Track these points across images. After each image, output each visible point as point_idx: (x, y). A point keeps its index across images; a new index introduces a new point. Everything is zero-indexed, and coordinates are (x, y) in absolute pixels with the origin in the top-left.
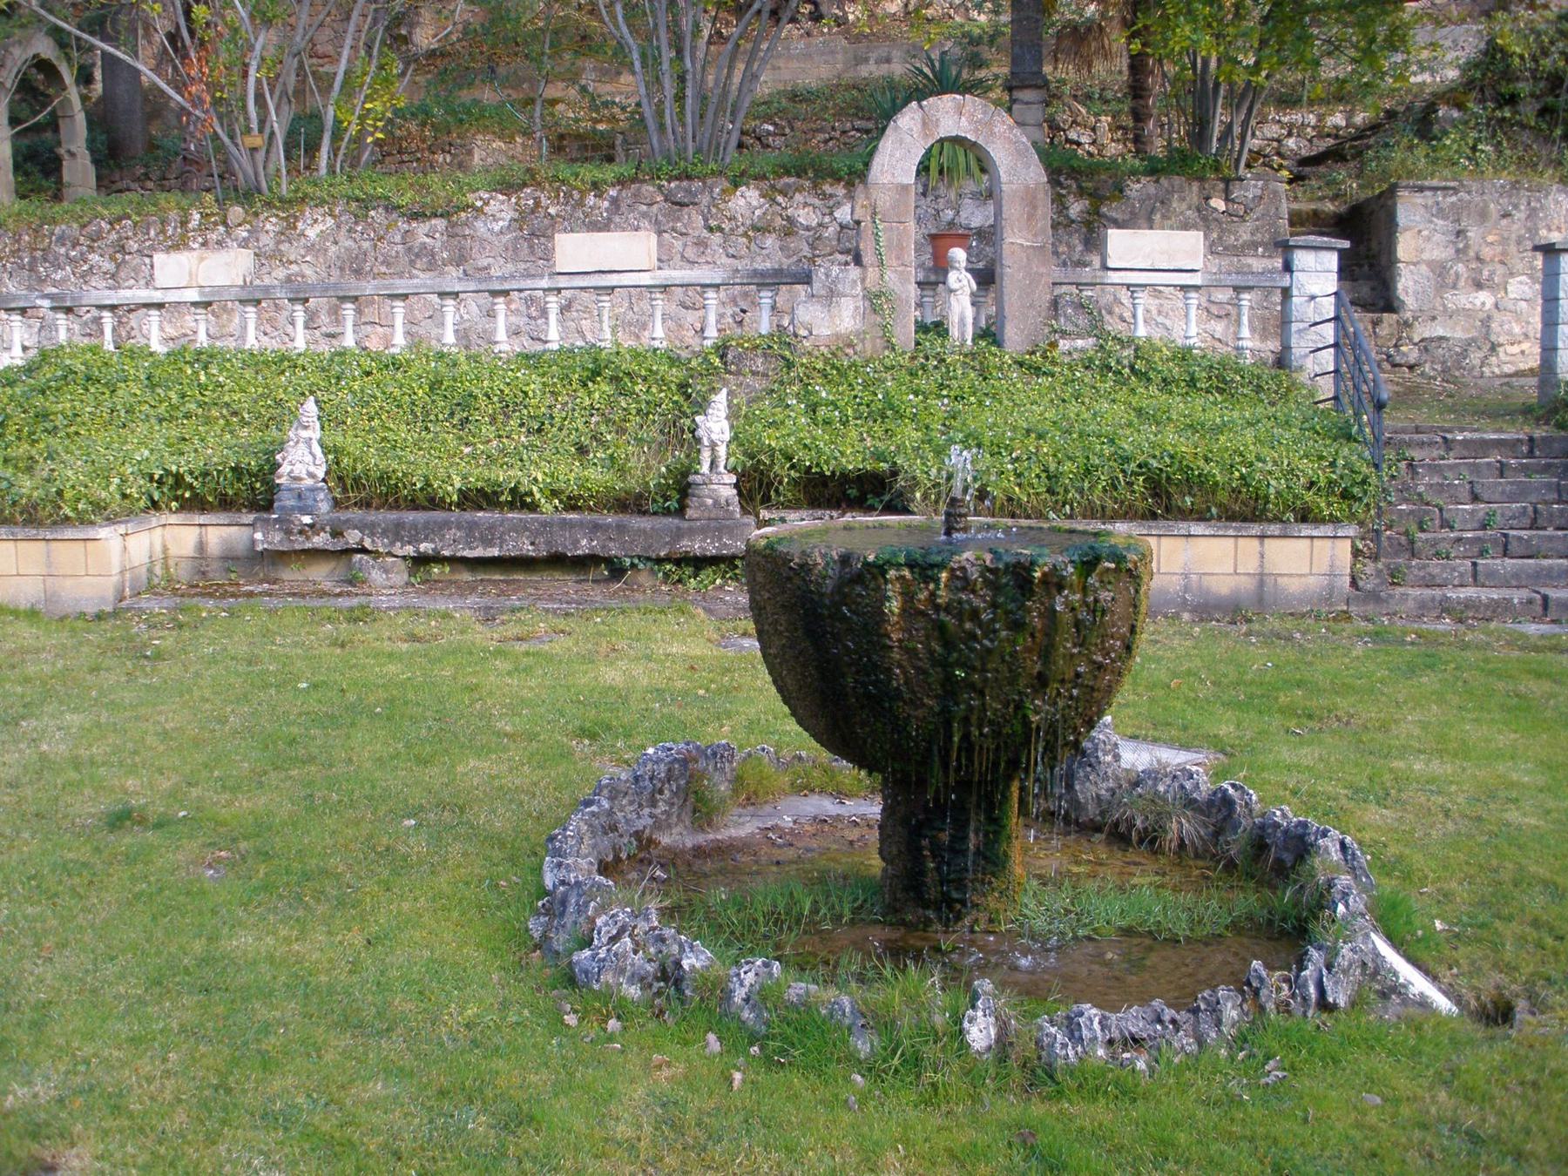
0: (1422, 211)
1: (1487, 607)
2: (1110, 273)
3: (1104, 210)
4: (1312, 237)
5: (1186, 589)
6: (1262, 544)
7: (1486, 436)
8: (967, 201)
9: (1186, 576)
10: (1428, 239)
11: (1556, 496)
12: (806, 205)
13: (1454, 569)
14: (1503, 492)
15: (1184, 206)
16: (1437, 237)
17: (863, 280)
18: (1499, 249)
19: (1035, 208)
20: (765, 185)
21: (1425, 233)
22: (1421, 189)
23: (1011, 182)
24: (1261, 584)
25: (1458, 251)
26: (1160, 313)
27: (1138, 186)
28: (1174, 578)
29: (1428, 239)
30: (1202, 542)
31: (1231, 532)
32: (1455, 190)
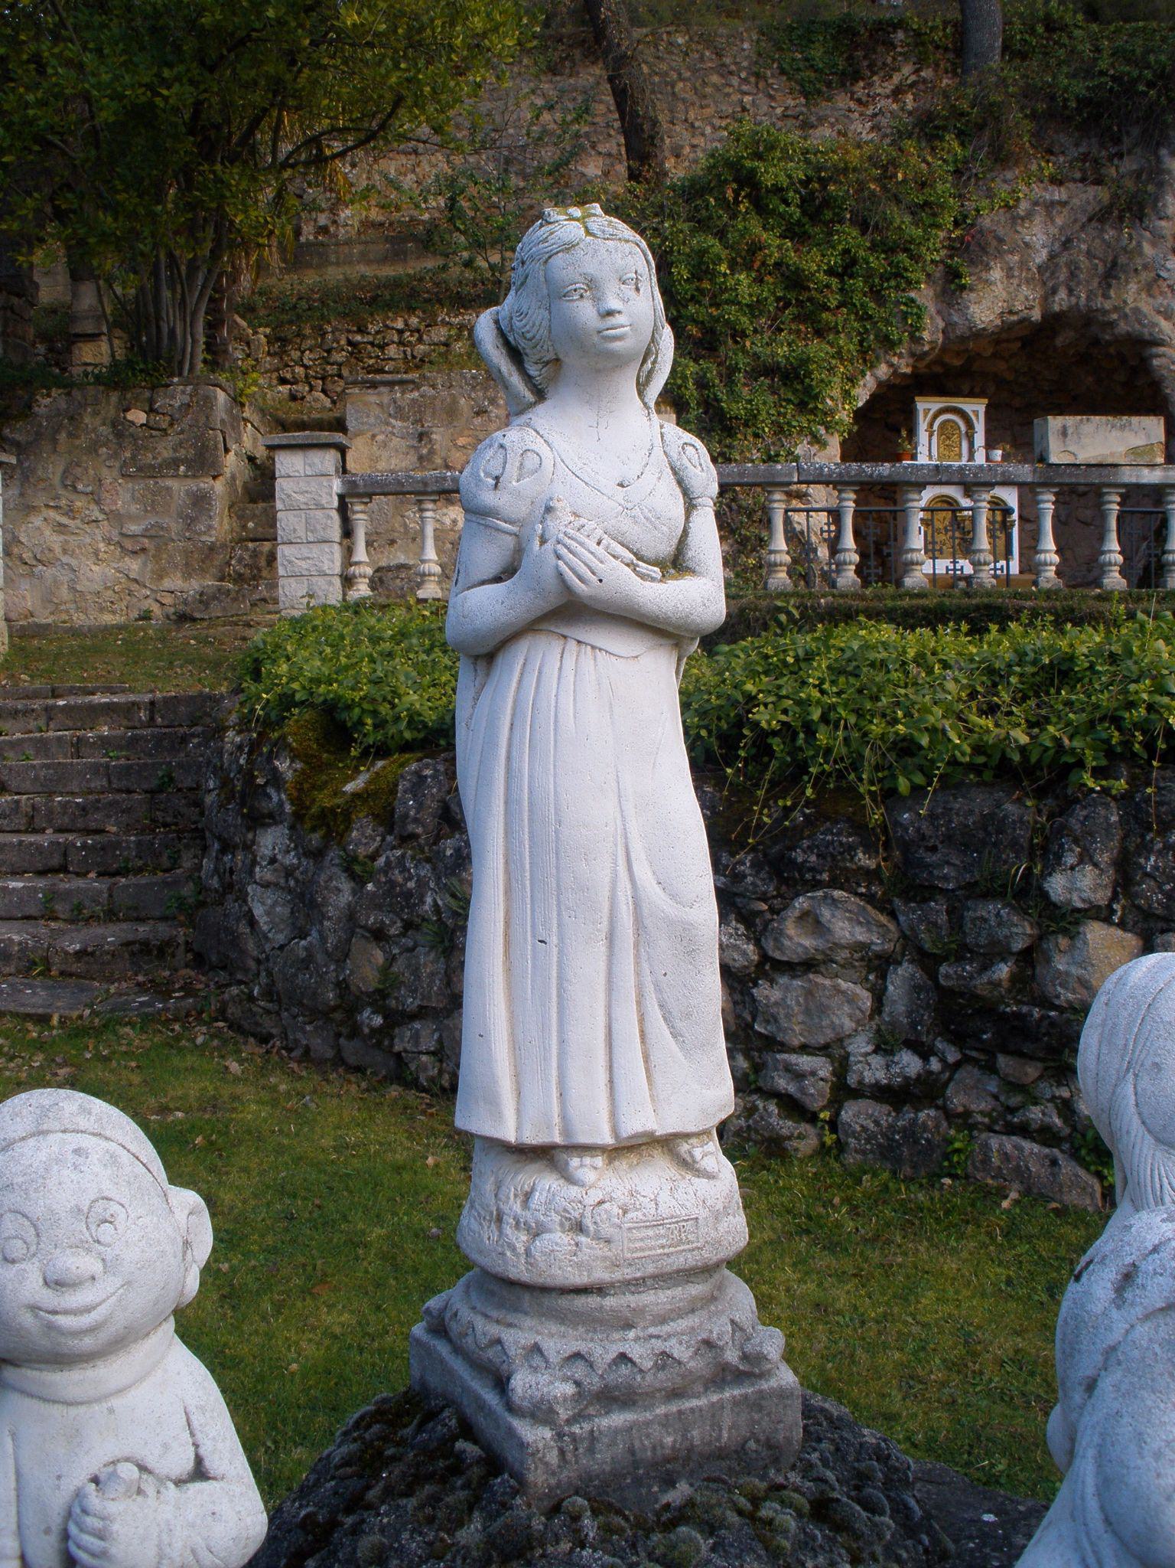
0: (377, 411)
10: (384, 445)
11: (105, 783)
14: (36, 778)
15: (98, 421)
16: (396, 442)
21: (380, 438)
22: (374, 385)
25: (421, 458)
26: (65, 551)
29: (384, 445)
32: (417, 386)
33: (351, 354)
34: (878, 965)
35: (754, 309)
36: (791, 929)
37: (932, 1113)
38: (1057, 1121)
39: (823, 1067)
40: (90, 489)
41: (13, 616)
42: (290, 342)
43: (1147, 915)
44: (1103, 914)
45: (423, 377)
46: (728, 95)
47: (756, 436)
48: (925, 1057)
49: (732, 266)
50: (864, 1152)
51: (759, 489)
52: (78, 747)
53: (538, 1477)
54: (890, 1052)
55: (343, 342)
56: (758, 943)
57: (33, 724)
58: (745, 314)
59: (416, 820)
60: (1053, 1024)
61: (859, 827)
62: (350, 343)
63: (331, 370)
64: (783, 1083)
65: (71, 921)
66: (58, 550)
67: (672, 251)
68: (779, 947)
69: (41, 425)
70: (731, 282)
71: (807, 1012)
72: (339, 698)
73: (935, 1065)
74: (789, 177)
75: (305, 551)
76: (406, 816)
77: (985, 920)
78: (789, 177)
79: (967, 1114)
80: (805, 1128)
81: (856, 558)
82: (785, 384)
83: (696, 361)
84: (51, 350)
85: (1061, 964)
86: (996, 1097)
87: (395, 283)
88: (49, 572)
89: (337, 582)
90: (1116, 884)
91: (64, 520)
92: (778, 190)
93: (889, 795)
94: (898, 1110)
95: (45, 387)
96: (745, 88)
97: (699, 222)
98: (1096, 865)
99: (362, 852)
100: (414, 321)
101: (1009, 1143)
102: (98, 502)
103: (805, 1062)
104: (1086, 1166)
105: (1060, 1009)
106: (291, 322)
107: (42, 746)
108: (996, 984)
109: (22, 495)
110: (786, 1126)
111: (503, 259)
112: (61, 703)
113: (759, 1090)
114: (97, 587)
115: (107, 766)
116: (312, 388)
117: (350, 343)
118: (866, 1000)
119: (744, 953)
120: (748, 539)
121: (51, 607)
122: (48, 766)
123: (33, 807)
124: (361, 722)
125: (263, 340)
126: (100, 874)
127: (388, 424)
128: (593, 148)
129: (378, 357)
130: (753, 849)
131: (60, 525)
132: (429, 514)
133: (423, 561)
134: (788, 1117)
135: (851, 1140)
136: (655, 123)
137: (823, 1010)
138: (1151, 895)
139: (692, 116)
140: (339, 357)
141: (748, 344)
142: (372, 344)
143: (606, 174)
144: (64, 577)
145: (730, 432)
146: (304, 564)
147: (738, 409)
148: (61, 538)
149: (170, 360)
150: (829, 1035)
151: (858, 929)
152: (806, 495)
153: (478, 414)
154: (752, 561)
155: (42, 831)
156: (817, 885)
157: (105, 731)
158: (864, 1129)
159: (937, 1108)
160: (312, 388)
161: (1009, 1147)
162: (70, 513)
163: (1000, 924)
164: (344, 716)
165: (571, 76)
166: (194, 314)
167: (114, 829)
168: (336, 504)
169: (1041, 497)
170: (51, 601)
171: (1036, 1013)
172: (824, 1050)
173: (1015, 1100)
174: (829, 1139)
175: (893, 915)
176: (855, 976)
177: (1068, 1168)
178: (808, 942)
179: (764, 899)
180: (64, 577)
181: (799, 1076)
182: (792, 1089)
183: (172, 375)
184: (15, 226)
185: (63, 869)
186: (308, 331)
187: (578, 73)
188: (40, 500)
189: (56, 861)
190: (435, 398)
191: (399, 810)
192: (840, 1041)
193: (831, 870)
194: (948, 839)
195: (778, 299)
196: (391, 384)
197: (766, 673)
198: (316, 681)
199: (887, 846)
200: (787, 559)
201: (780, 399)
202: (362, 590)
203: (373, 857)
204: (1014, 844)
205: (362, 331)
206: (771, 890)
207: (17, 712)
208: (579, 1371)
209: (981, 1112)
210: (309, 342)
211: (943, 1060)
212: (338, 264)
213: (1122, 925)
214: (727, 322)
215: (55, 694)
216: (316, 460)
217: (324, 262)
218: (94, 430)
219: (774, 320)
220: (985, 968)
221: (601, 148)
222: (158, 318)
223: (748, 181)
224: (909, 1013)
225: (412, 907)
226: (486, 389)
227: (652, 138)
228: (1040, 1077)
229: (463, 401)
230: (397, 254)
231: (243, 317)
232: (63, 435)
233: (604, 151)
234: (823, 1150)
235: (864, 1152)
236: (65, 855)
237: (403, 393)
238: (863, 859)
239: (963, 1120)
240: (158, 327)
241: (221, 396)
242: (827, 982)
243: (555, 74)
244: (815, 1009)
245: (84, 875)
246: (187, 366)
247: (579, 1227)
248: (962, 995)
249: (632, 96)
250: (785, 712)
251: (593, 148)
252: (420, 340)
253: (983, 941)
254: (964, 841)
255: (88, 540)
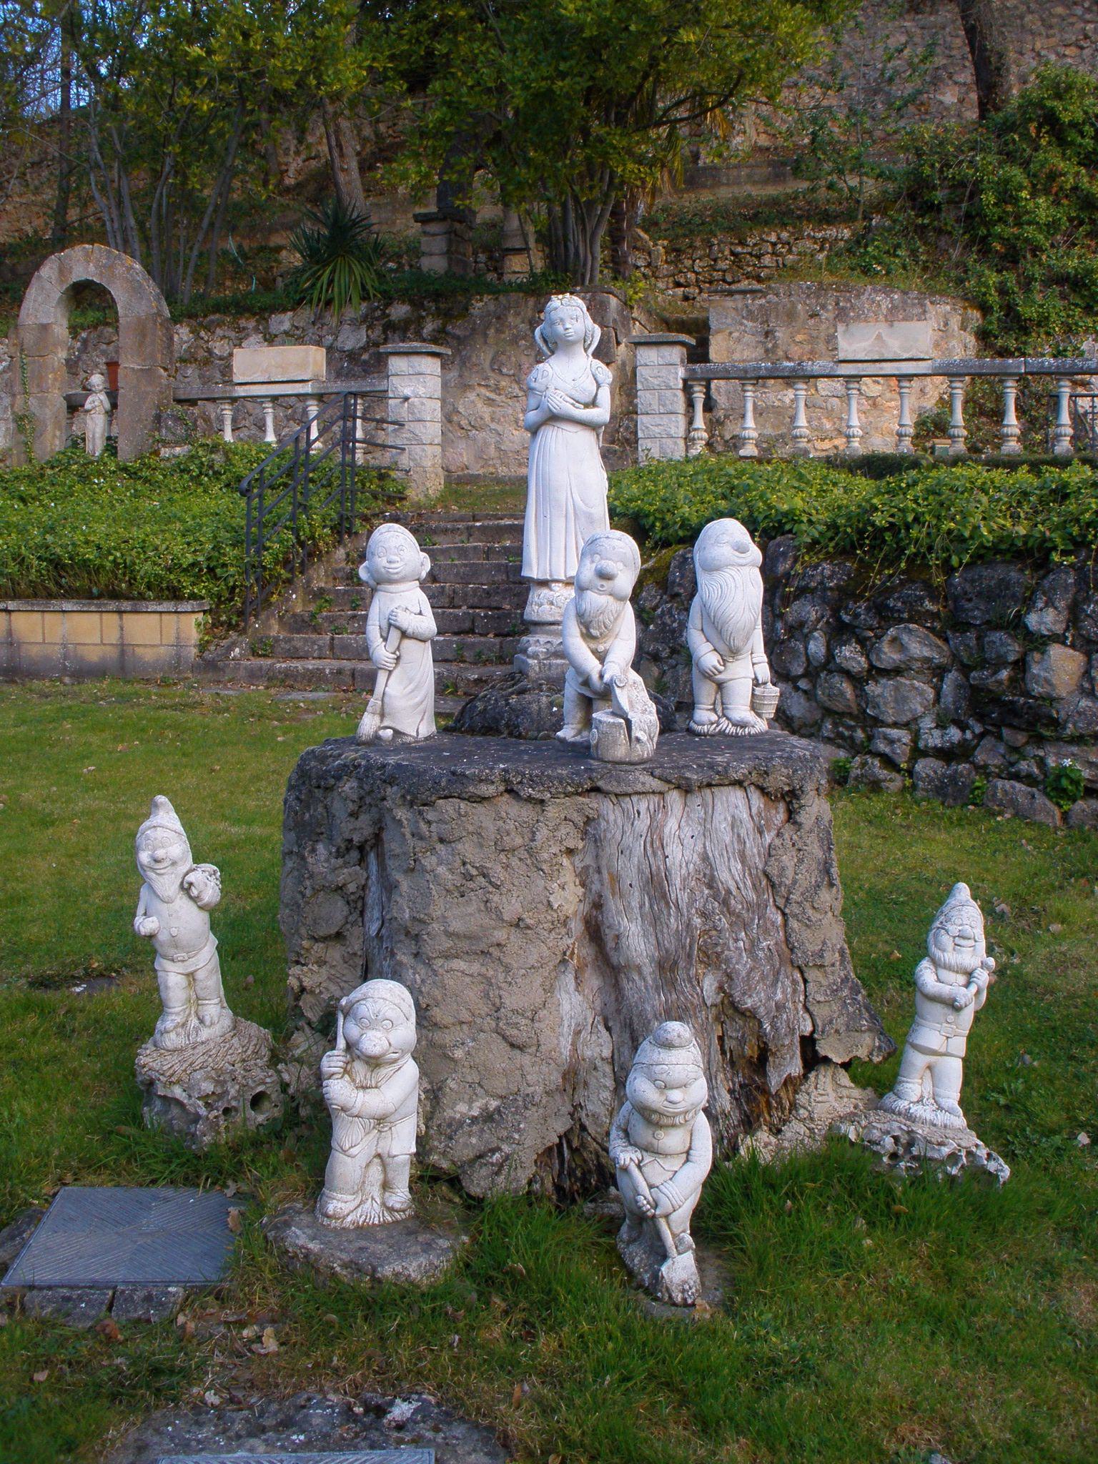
0: (733, 314)
1: (303, 676)
2: (237, 388)
3: (449, 328)
4: (415, 344)
5: (66, 657)
6: (121, 619)
7: (502, 522)
8: (347, 327)
9: (64, 645)
10: (739, 340)
11: (504, 577)
12: (224, 337)
13: (314, 643)
14: (458, 573)
15: (518, 320)
16: (747, 338)
17: (12, 406)
18: (808, 347)
19: (144, 336)
20: (193, 322)
21: (736, 335)
22: (731, 293)
23: (126, 316)
24: (123, 653)
25: (767, 351)
26: (492, 420)
27: (481, 304)
28: (57, 648)
29: (739, 340)
30: (76, 617)
31: (93, 608)
32: (763, 294)
33: (734, 262)
34: (939, 672)
35: (1052, 227)
36: (886, 647)
37: (967, 766)
38: (1036, 770)
39: (904, 736)
40: (512, 372)
41: (453, 468)
42: (684, 252)
43: (1089, 641)
44: (1059, 639)
45: (769, 288)
46: (1072, 24)
47: (1048, 334)
48: (963, 730)
49: (1034, 194)
50: (927, 791)
51: (1048, 378)
52: (488, 553)
53: (532, 674)
54: (945, 728)
55: (727, 253)
56: (868, 657)
57: (458, 538)
58: (1040, 233)
59: (680, 585)
60: (1030, 707)
61: (928, 586)
62: (733, 253)
63: (717, 275)
64: (882, 747)
65: (475, 664)
66: (487, 418)
67: (982, 180)
68: (879, 659)
69: (475, 323)
70: (1031, 205)
71: (896, 701)
72: (641, 510)
73: (969, 735)
74: (1086, 113)
75: (657, 419)
76: (674, 582)
77: (994, 642)
78: (1086, 113)
79: (986, 766)
80: (894, 775)
81: (1070, 431)
82: (1075, 291)
83: (999, 271)
84: (490, 258)
85: (1035, 670)
86: (1004, 756)
87: (774, 202)
88: (480, 435)
89: (681, 443)
90: (1068, 621)
91: (492, 396)
92: (1073, 125)
93: (948, 569)
94: (948, 765)
95: (478, 293)
96: (1088, 17)
97: (1008, 154)
98: (1056, 608)
99: (648, 605)
100: (785, 235)
101: (1008, 784)
102: (518, 382)
103: (895, 733)
104: (1051, 799)
105: (1033, 697)
106: (685, 236)
107: (463, 552)
108: (1000, 682)
109: (460, 376)
110: (883, 773)
111: (861, 183)
112: (478, 524)
113: (870, 752)
114: (517, 447)
115: (507, 566)
116: (701, 291)
117: (733, 253)
118: (931, 694)
119: (859, 663)
120: (1036, 419)
121: (482, 463)
122: (466, 565)
123: (454, 591)
124: (653, 525)
125: (662, 250)
126: (496, 635)
127: (742, 324)
128: (950, 78)
129: (754, 265)
130: (868, 600)
131: (489, 399)
132: (749, 394)
133: (745, 429)
134: (885, 768)
135: (920, 783)
136: (1001, 56)
137: (905, 700)
138: (1089, 627)
139: (1038, 45)
140: (723, 265)
141: (1044, 257)
142: (750, 254)
143: (961, 101)
144: (492, 439)
145: (1025, 331)
146: (657, 430)
147: (1029, 312)
148: (490, 409)
149: (575, 273)
150: (909, 716)
151: (925, 649)
152: (1089, 383)
153: (811, 317)
154: (1039, 437)
155: (460, 607)
156: (901, 621)
157: (508, 543)
158: (928, 776)
159: (971, 763)
160: (701, 291)
161: (1008, 787)
162: (497, 390)
163: (1002, 645)
164: (644, 521)
165: (931, 14)
166: (593, 235)
167: (508, 607)
168: (681, 385)
169: (1062, 383)
170: (481, 458)
171: (1022, 700)
172: (906, 725)
173: (1014, 757)
174: (908, 782)
175: (946, 640)
176: (925, 679)
177: (1041, 800)
178: (896, 656)
179: (872, 629)
180: (492, 439)
181: (891, 742)
182: (887, 750)
183: (576, 285)
184: (454, 177)
185: (471, 631)
186: (698, 244)
187: (937, 11)
188: (475, 380)
189: (467, 625)
190: (777, 304)
191: (671, 578)
192: (915, 720)
193: (909, 612)
194: (979, 594)
195: (1071, 220)
196: (744, 292)
197: (888, 493)
198: (630, 500)
199: (946, 598)
200: (1017, 431)
201: (1070, 304)
202: (698, 449)
203: (654, 609)
204: (1013, 596)
205: (742, 243)
206: (875, 623)
207: (447, 530)
208: (548, 646)
209: (995, 766)
210: (700, 253)
211: (973, 732)
212: (728, 185)
213: (1073, 646)
214: (1026, 240)
215: (475, 519)
216: (666, 354)
217: (717, 184)
218: (516, 327)
219: (1069, 236)
220: (995, 673)
221: (956, 78)
222: (566, 240)
223: (1051, 120)
224: (954, 703)
225: (674, 639)
226: (818, 297)
227: (998, 69)
228: (1027, 743)
229: (800, 307)
230: (777, 178)
231: (646, 231)
232: (492, 331)
233: (961, 80)
234: (904, 789)
235: (927, 791)
236: (473, 622)
237: (753, 300)
238: (928, 605)
239: (982, 769)
240: (566, 247)
241: (613, 301)
242: (908, 682)
243: (917, 13)
244: (901, 700)
245: (486, 635)
246: (588, 276)
247: (552, 603)
248: (982, 690)
249: (981, 32)
250: (892, 516)
251: (950, 78)
252: (790, 251)
253: (993, 656)
254: (988, 596)
255: (510, 411)
